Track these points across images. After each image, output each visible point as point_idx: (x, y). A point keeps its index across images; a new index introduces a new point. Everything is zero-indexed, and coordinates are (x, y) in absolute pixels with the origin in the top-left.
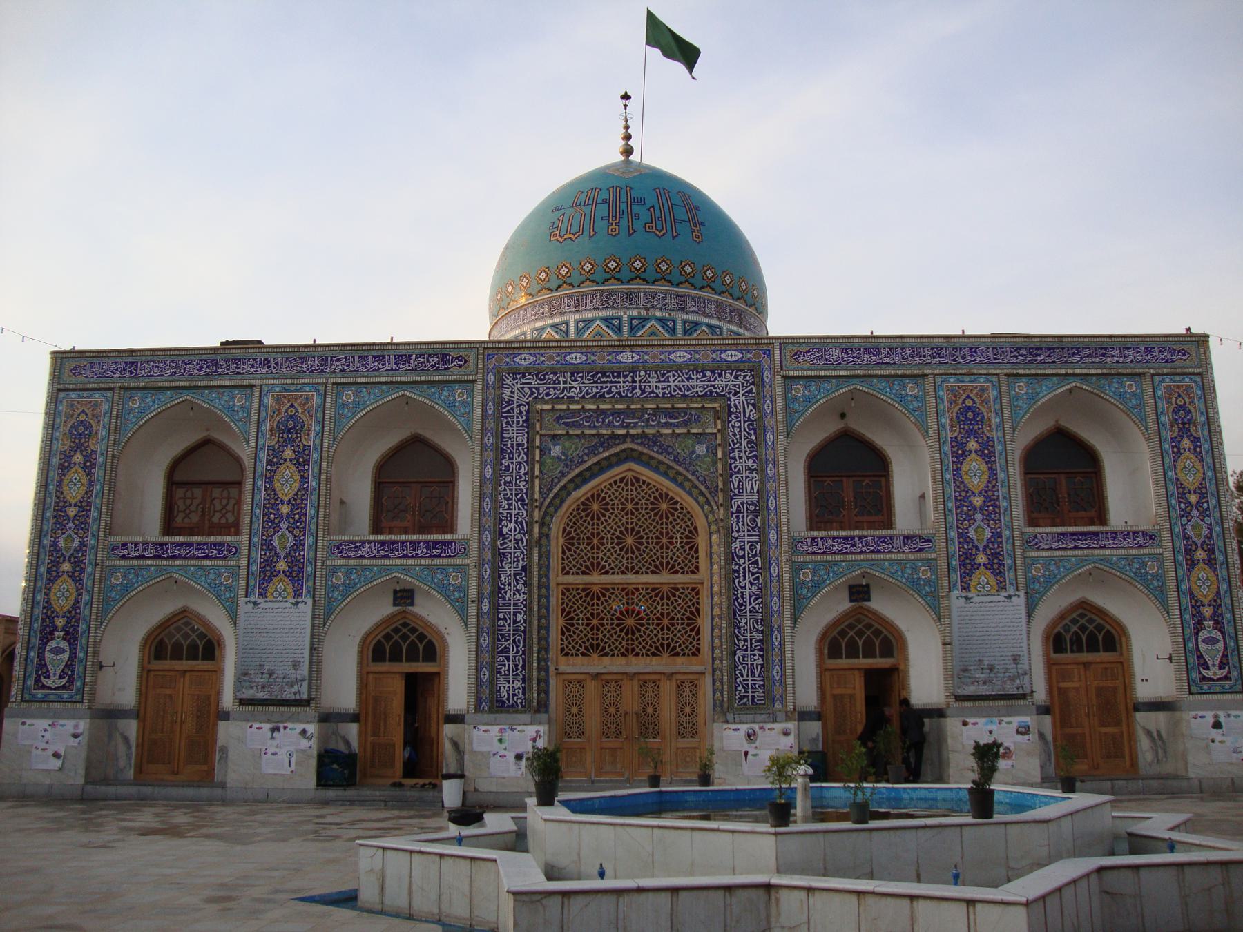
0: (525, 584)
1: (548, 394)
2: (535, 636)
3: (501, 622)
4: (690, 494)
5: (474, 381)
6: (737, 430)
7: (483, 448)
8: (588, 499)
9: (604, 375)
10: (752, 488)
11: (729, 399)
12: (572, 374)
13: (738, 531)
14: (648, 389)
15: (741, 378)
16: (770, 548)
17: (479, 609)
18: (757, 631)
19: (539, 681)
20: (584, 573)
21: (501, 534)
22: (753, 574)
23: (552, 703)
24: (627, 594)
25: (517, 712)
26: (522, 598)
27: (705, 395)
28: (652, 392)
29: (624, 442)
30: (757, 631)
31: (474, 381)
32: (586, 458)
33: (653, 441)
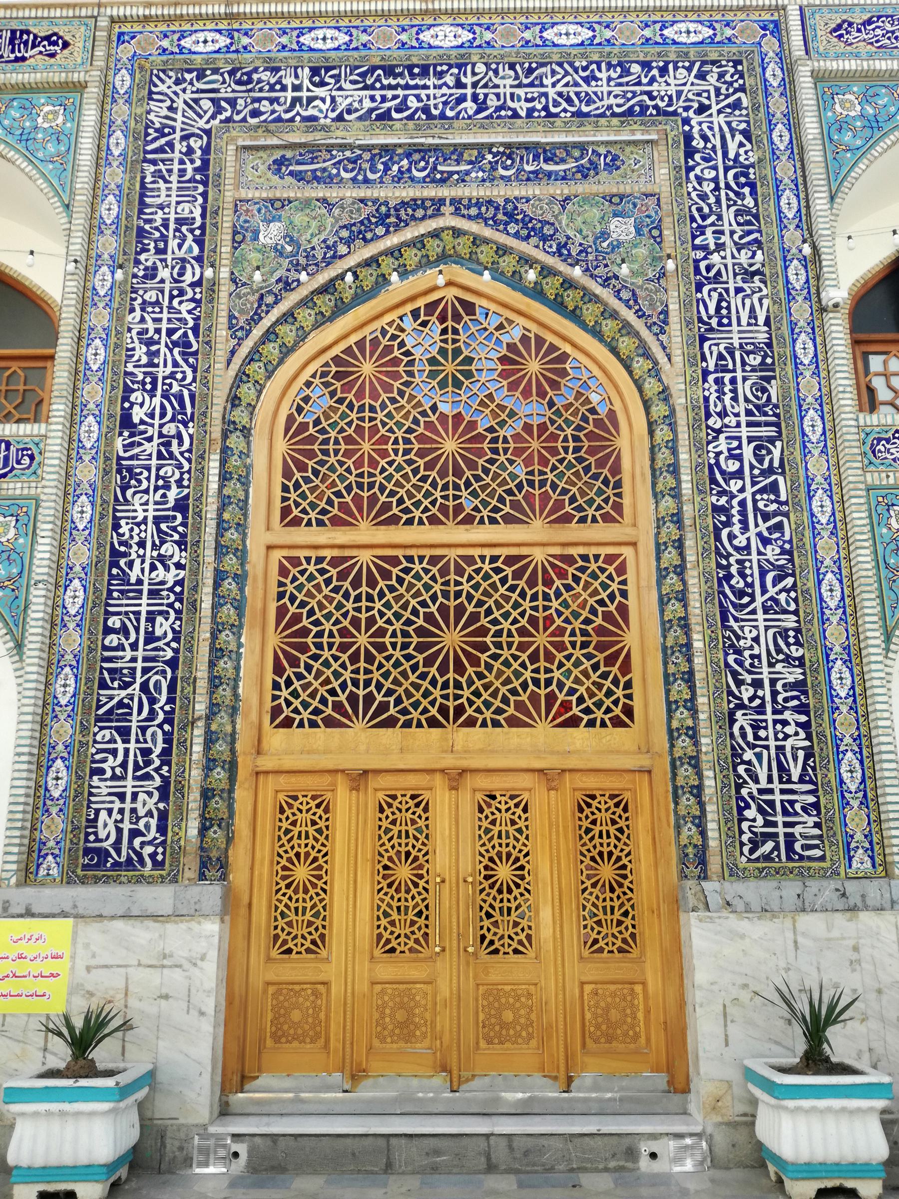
0: (181, 544)
1: (255, 113)
2: (202, 673)
3: (112, 640)
4: (596, 333)
5: (81, 87)
6: (708, 187)
7: (95, 227)
8: (348, 351)
9: (390, 71)
10: (753, 314)
11: (686, 121)
12: (315, 71)
13: (723, 414)
14: (492, 102)
15: (712, 78)
16: (806, 452)
17: (56, 607)
18: (788, 659)
19: (207, 794)
20: (337, 522)
21: (126, 421)
22: (766, 517)
23: (239, 856)
24: (444, 572)
25: (140, 880)
26: (171, 577)
27: (630, 112)
28: (502, 107)
29: (437, 213)
30: (788, 659)
31: (81, 87)
32: (342, 249)
33: (508, 214)
